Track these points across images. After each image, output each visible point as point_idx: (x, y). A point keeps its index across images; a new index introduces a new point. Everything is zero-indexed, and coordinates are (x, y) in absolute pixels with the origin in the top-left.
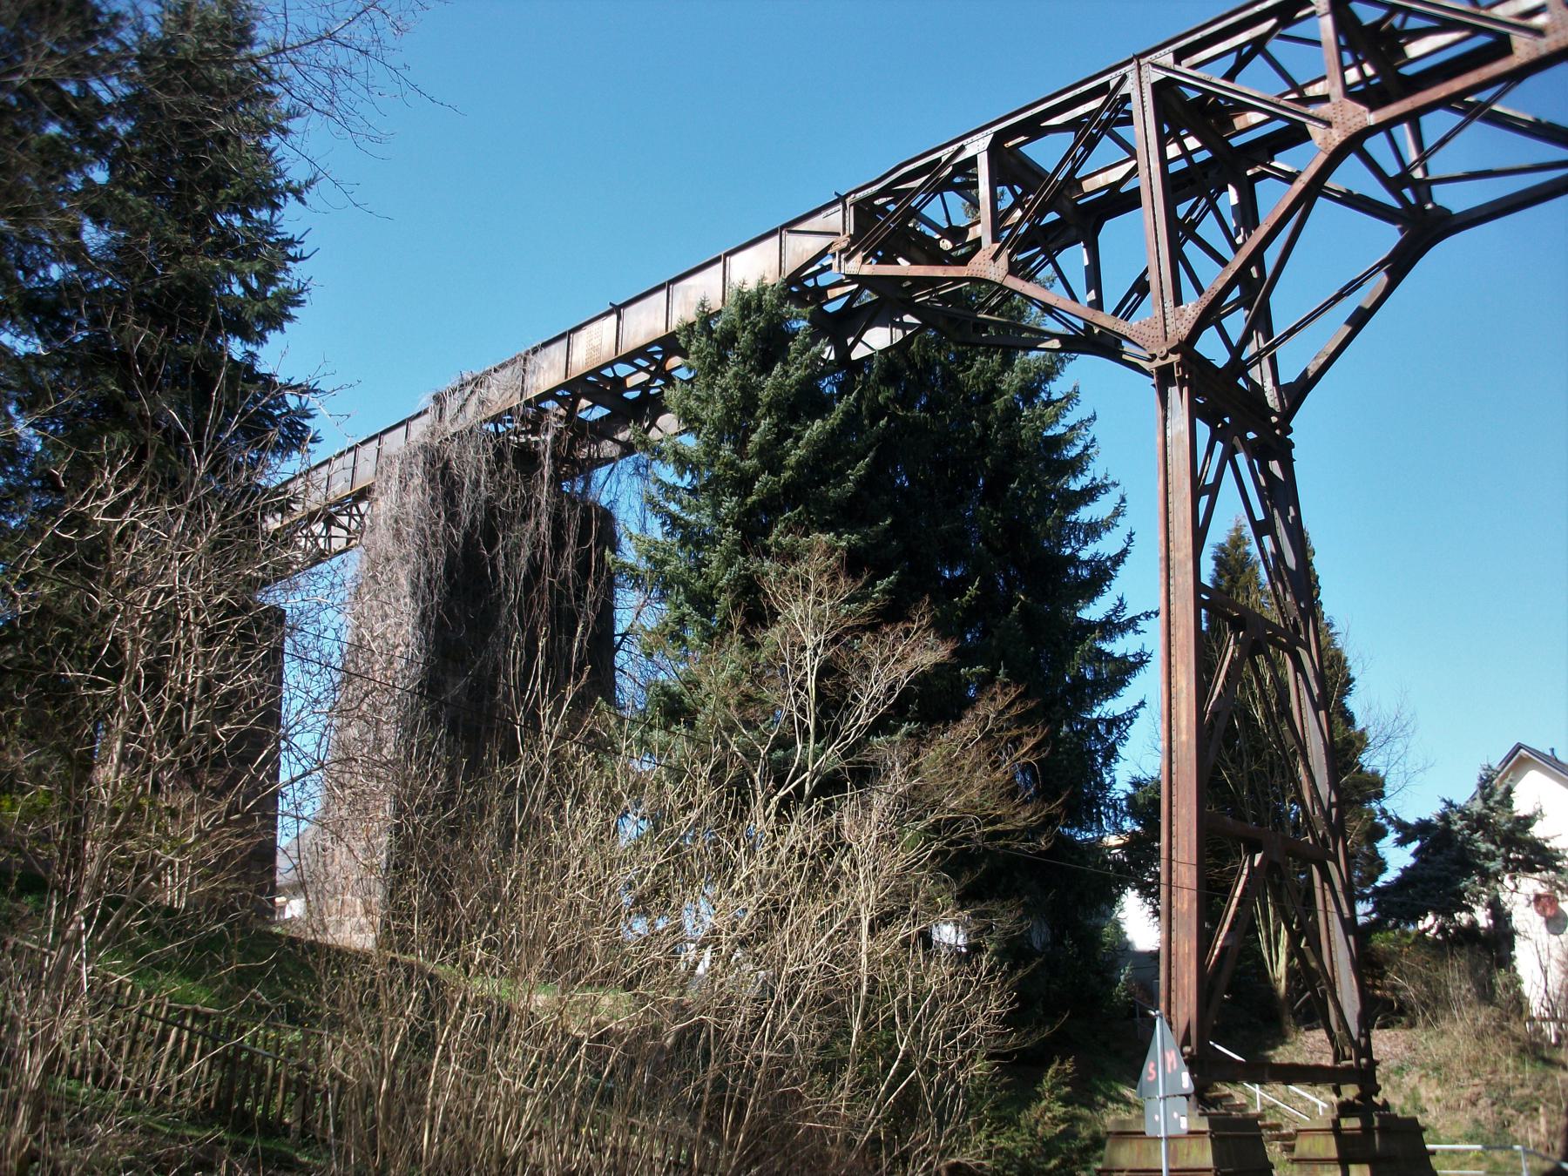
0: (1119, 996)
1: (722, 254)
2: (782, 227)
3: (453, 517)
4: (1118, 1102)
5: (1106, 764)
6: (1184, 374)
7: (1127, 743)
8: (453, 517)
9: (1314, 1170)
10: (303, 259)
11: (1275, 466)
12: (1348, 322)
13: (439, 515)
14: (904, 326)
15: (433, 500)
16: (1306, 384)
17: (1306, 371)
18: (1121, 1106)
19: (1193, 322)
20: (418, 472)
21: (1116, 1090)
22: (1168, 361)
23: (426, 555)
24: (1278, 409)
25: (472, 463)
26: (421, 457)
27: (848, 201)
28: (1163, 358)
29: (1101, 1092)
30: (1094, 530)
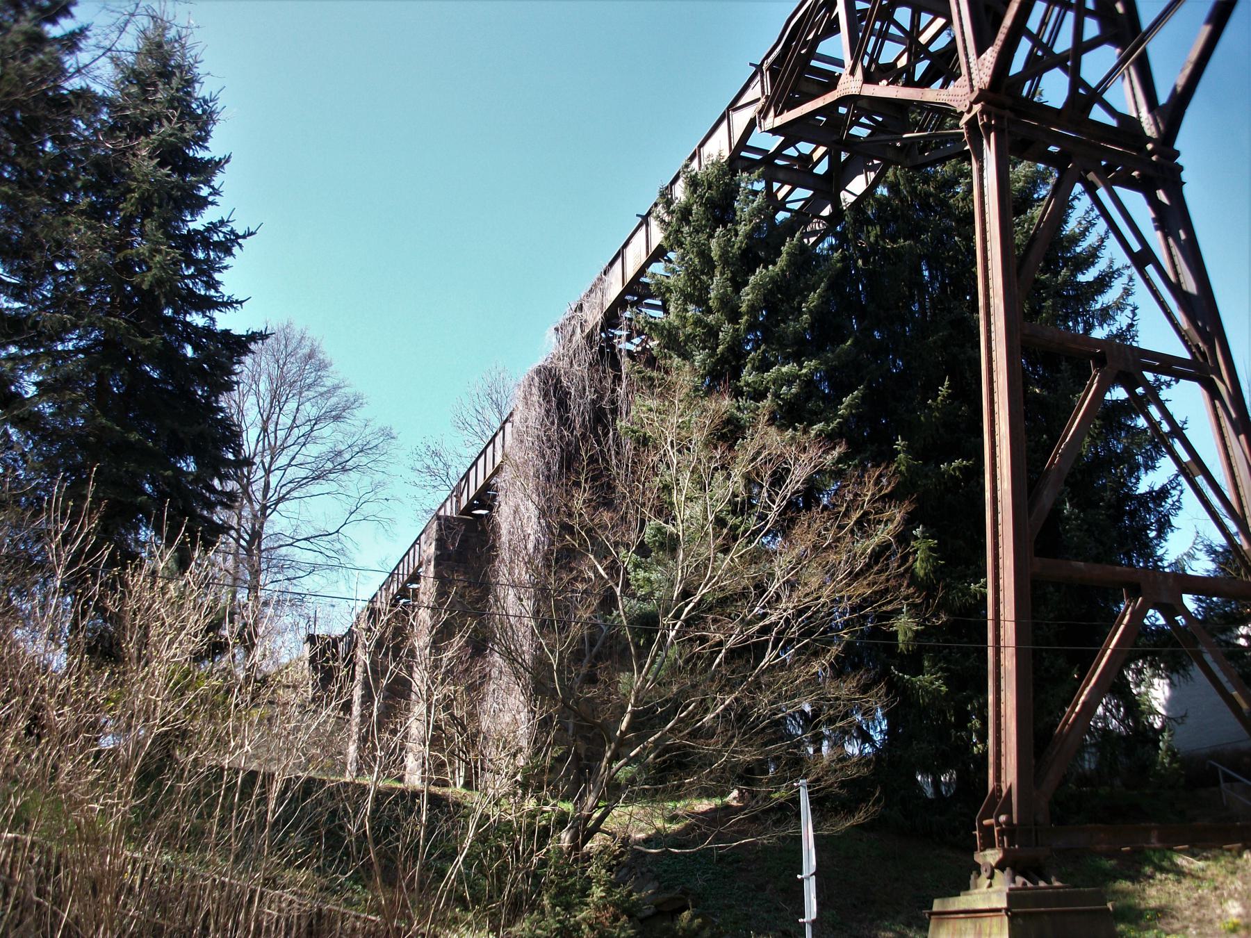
0: (1163, 763)
1: (696, 147)
2: (728, 109)
3: (565, 422)
4: (1168, 871)
5: (1161, 535)
6: (989, 119)
7: (1179, 512)
8: (565, 422)
9: (979, 933)
10: (251, 234)
11: (1161, 195)
12: (1208, 21)
13: (553, 423)
14: (873, 168)
15: (548, 411)
16: (1182, 98)
17: (1175, 89)
18: (1171, 876)
19: (992, 66)
20: (535, 390)
21: (1171, 860)
22: (973, 113)
23: (543, 456)
24: (1155, 136)
25: (577, 373)
26: (537, 379)
27: (764, 68)
28: (969, 111)
29: (1151, 862)
30: (1105, 315)
